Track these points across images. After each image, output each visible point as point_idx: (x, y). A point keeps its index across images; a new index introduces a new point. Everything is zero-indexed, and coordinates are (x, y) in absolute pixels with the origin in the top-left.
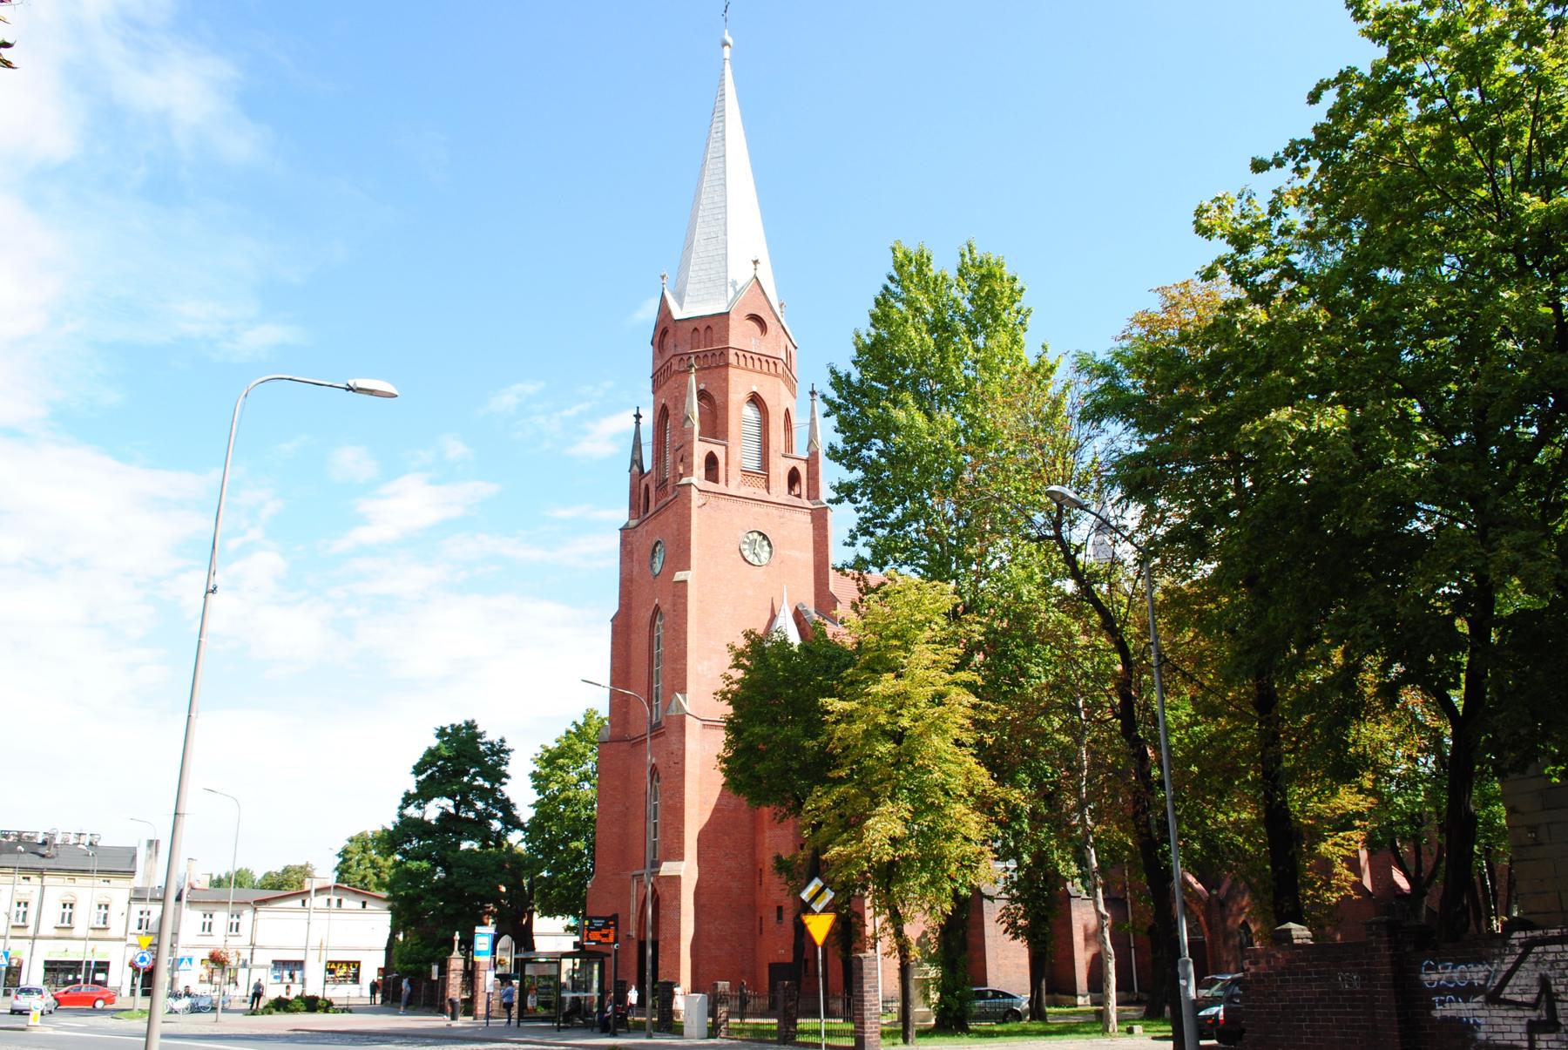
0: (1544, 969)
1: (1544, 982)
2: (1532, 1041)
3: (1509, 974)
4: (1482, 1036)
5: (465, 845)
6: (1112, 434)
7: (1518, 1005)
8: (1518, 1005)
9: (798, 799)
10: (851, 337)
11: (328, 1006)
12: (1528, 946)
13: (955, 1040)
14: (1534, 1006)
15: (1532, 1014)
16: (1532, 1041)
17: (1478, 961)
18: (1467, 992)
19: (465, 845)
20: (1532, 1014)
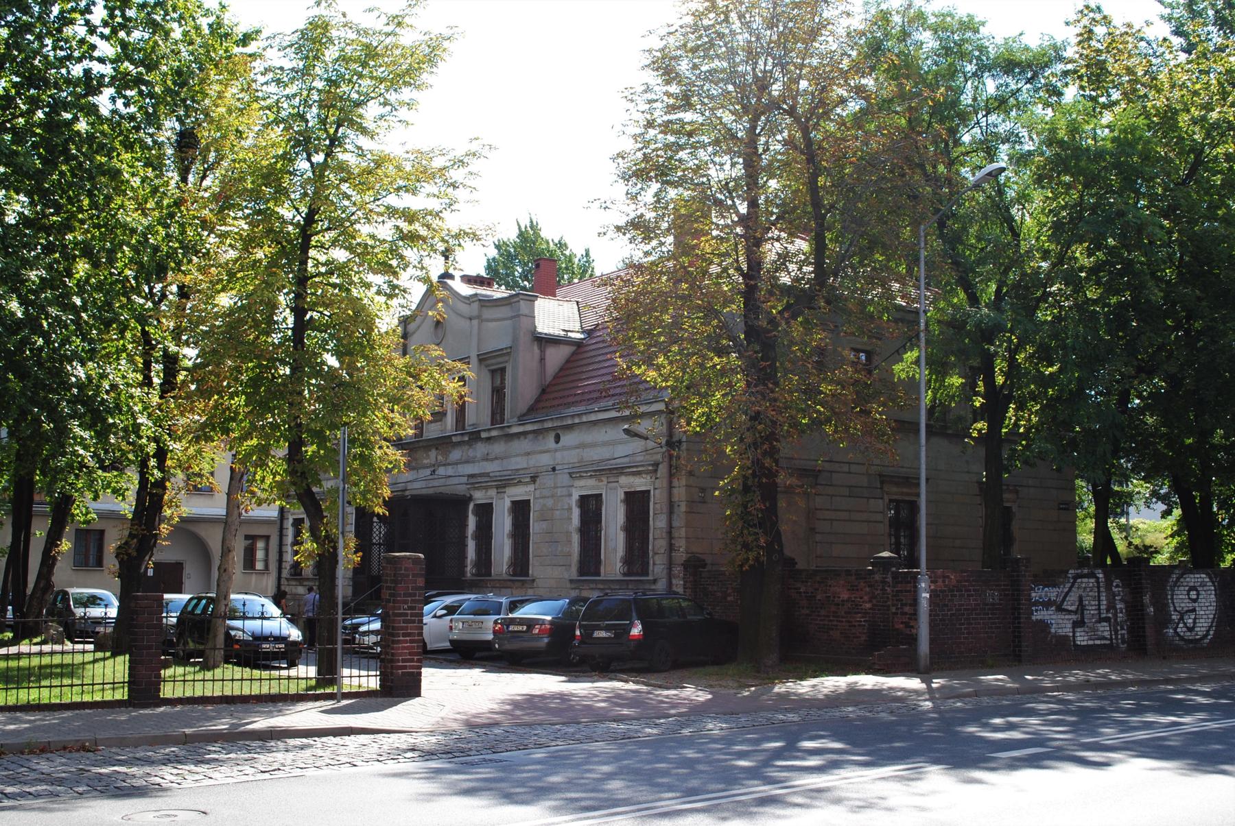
0: (1081, 592)
1: (1081, 599)
2: (1074, 632)
3: (1067, 594)
4: (1053, 631)
5: (1191, 441)
6: (65, 648)
7: (1069, 612)
8: (1069, 612)
9: (339, 385)
10: (257, 26)
11: (53, 538)
12: (1076, 577)
13: (951, 745)
14: (1075, 612)
15: (1074, 617)
16: (1074, 632)
17: (1054, 586)
18: (1047, 604)
19: (1191, 441)
20: (1074, 617)
